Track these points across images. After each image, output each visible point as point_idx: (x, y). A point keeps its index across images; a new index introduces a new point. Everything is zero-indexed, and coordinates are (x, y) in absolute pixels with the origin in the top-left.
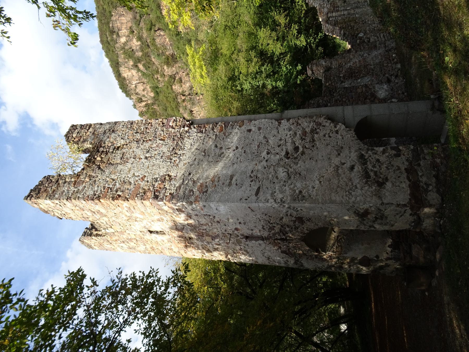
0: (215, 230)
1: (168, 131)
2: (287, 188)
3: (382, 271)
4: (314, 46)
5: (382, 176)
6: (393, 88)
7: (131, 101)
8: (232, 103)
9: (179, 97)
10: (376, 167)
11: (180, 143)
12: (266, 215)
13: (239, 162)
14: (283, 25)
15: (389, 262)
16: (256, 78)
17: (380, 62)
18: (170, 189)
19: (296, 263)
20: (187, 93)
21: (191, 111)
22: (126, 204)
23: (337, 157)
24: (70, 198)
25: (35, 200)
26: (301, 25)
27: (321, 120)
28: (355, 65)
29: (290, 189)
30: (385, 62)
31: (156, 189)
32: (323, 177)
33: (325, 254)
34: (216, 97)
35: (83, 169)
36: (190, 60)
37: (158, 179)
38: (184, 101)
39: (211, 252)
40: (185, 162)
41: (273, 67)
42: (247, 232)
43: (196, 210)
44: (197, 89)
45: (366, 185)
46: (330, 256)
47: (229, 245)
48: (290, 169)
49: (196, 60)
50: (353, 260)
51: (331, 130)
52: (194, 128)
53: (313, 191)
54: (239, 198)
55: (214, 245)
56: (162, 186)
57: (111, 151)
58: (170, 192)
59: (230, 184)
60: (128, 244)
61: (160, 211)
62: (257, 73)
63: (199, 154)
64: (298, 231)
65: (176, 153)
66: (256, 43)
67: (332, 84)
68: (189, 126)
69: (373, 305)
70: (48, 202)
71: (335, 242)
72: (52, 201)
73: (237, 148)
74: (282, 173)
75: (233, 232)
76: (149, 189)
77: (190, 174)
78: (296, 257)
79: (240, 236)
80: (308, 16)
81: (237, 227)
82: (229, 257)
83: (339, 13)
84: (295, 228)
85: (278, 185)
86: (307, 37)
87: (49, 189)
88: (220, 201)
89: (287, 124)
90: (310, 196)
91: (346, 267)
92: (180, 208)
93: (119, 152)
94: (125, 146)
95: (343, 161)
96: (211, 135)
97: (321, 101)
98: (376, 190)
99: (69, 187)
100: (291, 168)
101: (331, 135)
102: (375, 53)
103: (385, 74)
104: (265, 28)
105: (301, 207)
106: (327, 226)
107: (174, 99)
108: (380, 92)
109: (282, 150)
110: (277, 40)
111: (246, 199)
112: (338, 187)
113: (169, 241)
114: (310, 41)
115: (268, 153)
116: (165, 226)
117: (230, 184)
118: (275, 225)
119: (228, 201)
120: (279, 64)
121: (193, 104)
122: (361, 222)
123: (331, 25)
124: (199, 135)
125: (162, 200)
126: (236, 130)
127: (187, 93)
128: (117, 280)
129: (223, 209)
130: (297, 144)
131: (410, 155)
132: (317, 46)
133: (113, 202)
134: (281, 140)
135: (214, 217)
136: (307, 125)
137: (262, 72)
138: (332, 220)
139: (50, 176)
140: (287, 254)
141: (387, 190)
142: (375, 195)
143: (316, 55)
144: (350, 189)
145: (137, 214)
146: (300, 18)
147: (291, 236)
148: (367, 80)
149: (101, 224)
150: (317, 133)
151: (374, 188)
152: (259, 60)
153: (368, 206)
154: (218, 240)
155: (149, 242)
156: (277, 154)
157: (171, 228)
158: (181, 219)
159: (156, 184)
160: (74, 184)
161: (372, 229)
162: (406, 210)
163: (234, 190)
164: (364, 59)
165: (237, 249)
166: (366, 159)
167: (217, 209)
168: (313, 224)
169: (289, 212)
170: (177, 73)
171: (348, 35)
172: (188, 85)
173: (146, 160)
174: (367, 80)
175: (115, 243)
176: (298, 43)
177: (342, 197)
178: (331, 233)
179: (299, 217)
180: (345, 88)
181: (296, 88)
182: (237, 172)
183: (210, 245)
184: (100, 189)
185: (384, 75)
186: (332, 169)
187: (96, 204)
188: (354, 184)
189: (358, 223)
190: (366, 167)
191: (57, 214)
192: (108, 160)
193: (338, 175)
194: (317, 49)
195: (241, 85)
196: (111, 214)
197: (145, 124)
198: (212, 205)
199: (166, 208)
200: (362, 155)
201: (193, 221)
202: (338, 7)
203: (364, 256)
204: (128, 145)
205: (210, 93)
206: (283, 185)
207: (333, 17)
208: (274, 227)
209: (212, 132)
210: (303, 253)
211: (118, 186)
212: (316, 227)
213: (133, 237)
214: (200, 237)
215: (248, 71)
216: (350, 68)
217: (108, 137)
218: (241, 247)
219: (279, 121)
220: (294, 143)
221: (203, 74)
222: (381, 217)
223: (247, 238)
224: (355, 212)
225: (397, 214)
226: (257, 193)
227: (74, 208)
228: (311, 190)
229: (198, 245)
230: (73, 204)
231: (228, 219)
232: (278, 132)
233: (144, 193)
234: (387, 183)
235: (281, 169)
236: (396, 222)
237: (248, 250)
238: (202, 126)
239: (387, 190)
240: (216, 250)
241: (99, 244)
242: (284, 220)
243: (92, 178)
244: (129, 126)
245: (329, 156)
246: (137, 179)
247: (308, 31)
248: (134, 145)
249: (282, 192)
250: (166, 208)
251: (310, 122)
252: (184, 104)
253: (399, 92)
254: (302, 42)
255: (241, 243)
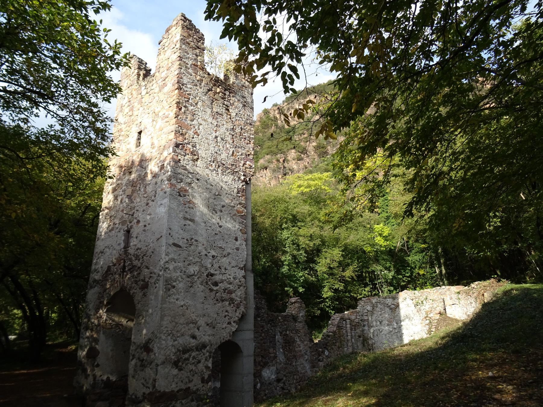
0: (138, 200)
1: (241, 160)
2: (179, 274)
3: (80, 371)
4: (322, 305)
5: (184, 365)
6: (271, 384)
7: (282, 102)
8: (269, 218)
9: (282, 155)
10: (193, 359)
11: (229, 171)
12: (153, 252)
13: (206, 228)
14: (344, 274)
15: (91, 378)
16: (294, 244)
17: (298, 372)
18: (184, 159)
19: (95, 281)
20: (286, 165)
21: (266, 168)
22: (172, 114)
23: (206, 323)
24: (181, 60)
25: (180, 25)
26: (343, 292)
27: (242, 309)
28: (297, 346)
29: (178, 277)
30: (298, 377)
31: (186, 146)
32: (187, 309)
33: (105, 311)
34: (277, 201)
35: (209, 74)
36: (317, 175)
37: (195, 149)
38: (278, 161)
39: (113, 192)
40: (210, 175)
41: (303, 262)
42: (135, 232)
43: (161, 184)
44: (290, 178)
45: (176, 350)
46: (101, 317)
47: (120, 213)
48: (196, 277)
49: (316, 182)
50: (96, 341)
51: (231, 318)
52: (243, 186)
53: (174, 299)
54: (171, 227)
55: (121, 197)
56: (187, 152)
57: (225, 102)
58: (182, 159)
59: (185, 219)
60: (126, 105)
61: (162, 147)
62: (298, 246)
63: (217, 190)
64: (132, 283)
65: (219, 167)
66: (328, 246)
67: (280, 322)
68: (245, 181)
69: (23, 371)
70: (178, 37)
71: (116, 322)
72: (179, 41)
73: (220, 227)
74: (193, 269)
75: (136, 218)
76: (185, 139)
77: (198, 180)
78: (102, 281)
79: (131, 224)
80: (352, 301)
81: (141, 222)
82: (106, 211)
83: (349, 331)
84: (136, 281)
85: (182, 265)
86: (332, 299)
87: (191, 39)
88: (170, 208)
89: (241, 276)
90: (169, 296)
91: (88, 334)
92: (165, 169)
93: (224, 111)
94: (229, 116)
95: (201, 328)
96: (234, 202)
97: (263, 311)
98: (171, 359)
99: (192, 59)
100: (198, 278)
101: (227, 317)
102: (308, 366)
103: (286, 377)
104: (342, 255)
105: (159, 288)
106: (137, 313)
107: (280, 150)
108: (268, 372)
109: (216, 270)
110: (330, 268)
111: (170, 234)
112: (177, 323)
113: (128, 150)
114: (327, 302)
115: (213, 256)
116: (146, 149)
117: (185, 219)
118: (141, 261)
119: (170, 216)
120: (306, 269)
121: (274, 171)
122: (138, 346)
123: (339, 323)
124: (236, 190)
125: (174, 151)
126: (237, 227)
127: (286, 165)
128: (105, 116)
129: (162, 211)
130: (220, 285)
131: (202, 392)
132: (321, 309)
133: (175, 102)
134: (226, 269)
135: (153, 201)
136: (238, 295)
137: (299, 250)
138: (143, 317)
139: (204, 40)
140: (107, 272)
141: (170, 370)
142: (166, 359)
143: (312, 307)
144: (173, 335)
145: (160, 123)
146: (350, 292)
147: (128, 276)
148: (281, 358)
149: (151, 84)
150: (230, 304)
151: (173, 357)
152: (311, 248)
153: (156, 351)
154: (127, 201)
155: (128, 128)
156: (212, 266)
157: (143, 155)
158: (153, 167)
159: (190, 146)
160: (194, 65)
161: (131, 358)
162: (149, 388)
163: (179, 222)
164: (302, 356)
165: (115, 220)
166: (201, 350)
167: (161, 204)
168: (139, 298)
169: (154, 275)
170: (308, 156)
171: (327, 340)
172: (295, 167)
173: (214, 137)
174: (281, 358)
175: (129, 92)
176: (326, 289)
177: (166, 327)
178: (126, 318)
179: (148, 285)
180: (275, 335)
181: (280, 286)
182: (197, 225)
183: (121, 193)
184: (188, 90)
185: (285, 375)
186: (194, 318)
187: (173, 85)
188: (178, 339)
189: (139, 344)
190: (193, 350)
191: (164, 41)
192: (216, 100)
193: (187, 324)
194: (318, 309)
195: (287, 228)
196: (162, 96)
197: (249, 137)
198: (166, 201)
199: (165, 154)
200: (206, 347)
201: (150, 179)
202: (355, 330)
203: (99, 352)
204: (229, 120)
205: (281, 195)
206: (182, 270)
207: (346, 325)
208: (139, 260)
209: (238, 203)
210: (107, 289)
211: (191, 108)
212: (136, 302)
213: (135, 113)
214: (131, 183)
215: (301, 236)
216: (294, 341)
217: (239, 101)
218: (117, 225)
219: (244, 268)
220: (222, 281)
221: (302, 188)
222: (143, 365)
223: (128, 231)
224: (150, 339)
225: (146, 380)
226: (175, 245)
227: (170, 60)
228: (175, 297)
229: (122, 180)
230: (174, 62)
231: (150, 214)
232: (233, 267)
233: (182, 134)
234: (177, 370)
235: (197, 268)
236: (137, 380)
237: (113, 232)
238: (244, 194)
239: (170, 370)
240: (116, 198)
241: (128, 74)
242: (146, 270)
243: (199, 82)
244: (248, 122)
245: (207, 315)
246: (196, 127)
247: (336, 300)
248: (230, 126)
249: (175, 269)
250: (165, 154)
251: (241, 298)
252: (274, 161)
253: (267, 391)
254: (327, 293)
255: (122, 225)
